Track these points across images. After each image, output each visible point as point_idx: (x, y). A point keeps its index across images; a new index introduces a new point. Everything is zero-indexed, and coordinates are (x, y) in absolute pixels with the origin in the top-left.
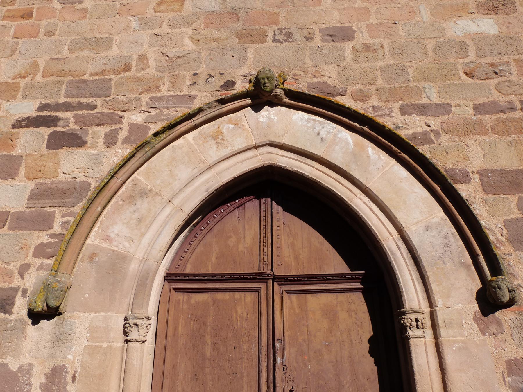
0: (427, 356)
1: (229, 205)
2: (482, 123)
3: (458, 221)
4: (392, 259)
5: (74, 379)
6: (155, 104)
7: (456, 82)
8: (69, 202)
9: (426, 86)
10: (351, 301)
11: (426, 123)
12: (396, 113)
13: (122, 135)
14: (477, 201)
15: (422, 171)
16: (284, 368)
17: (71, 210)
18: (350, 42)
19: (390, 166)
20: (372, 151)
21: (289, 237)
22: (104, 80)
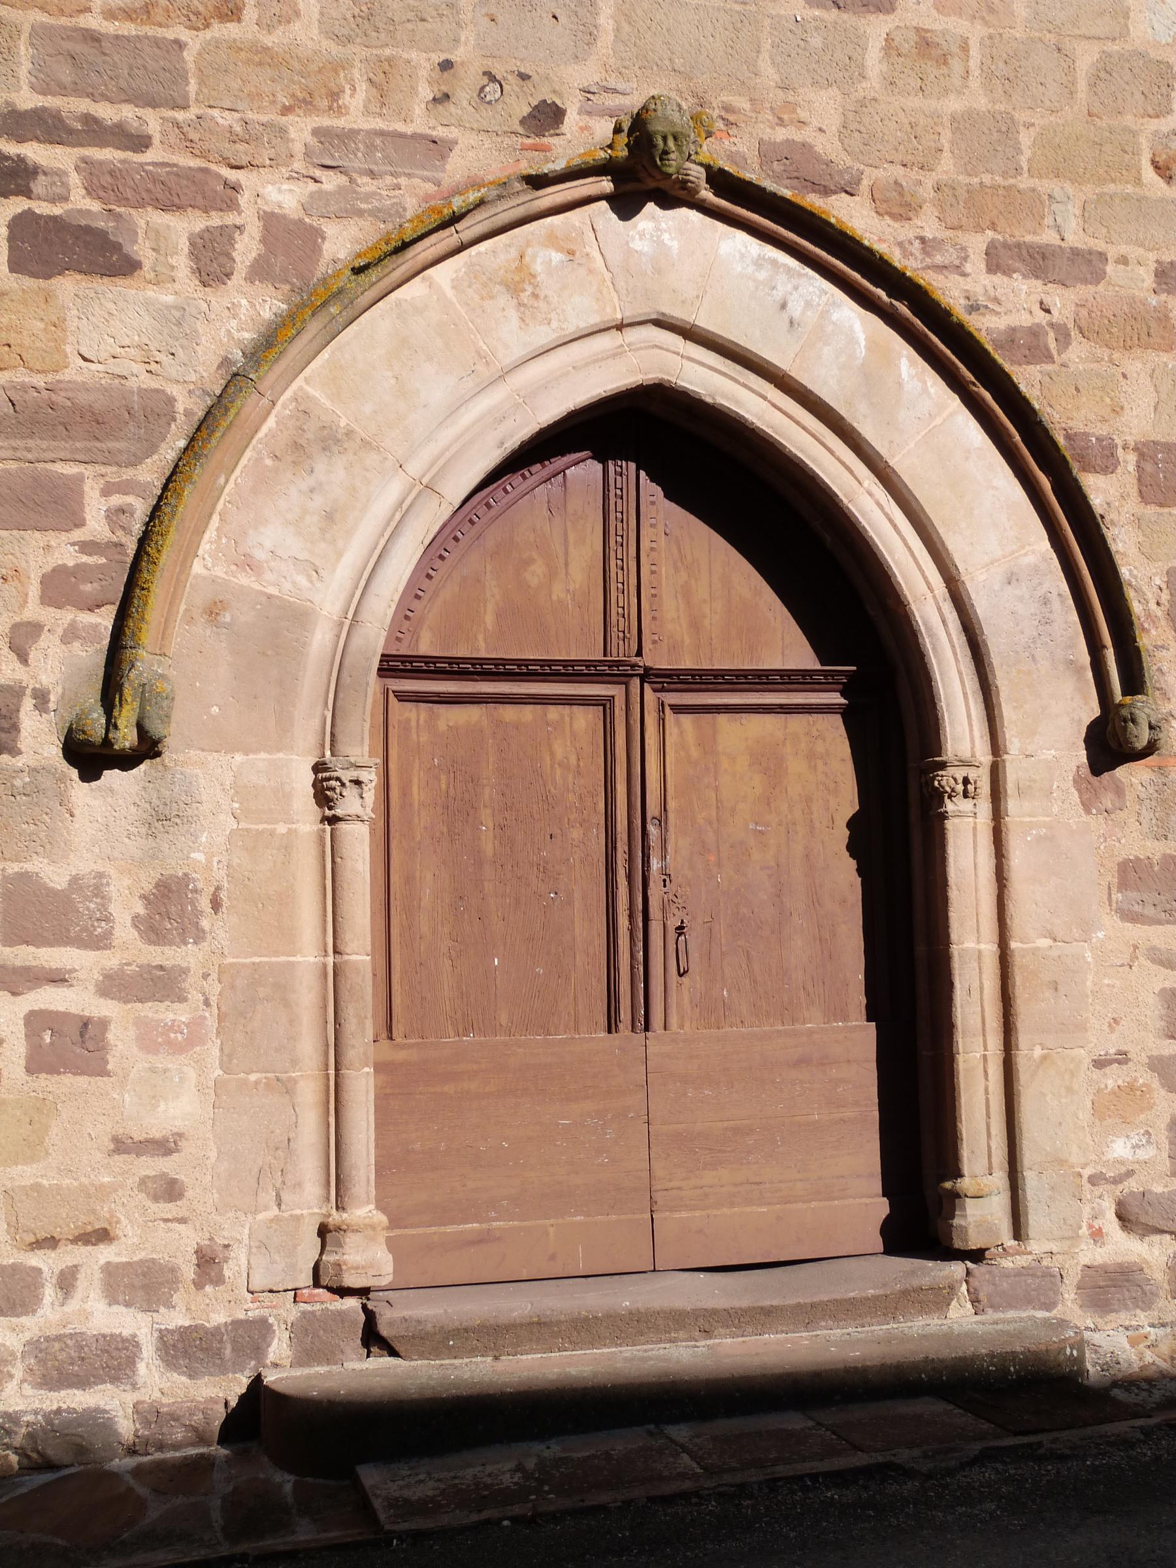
0: (975, 852)
1: (527, 473)
2: (1167, 317)
3: (1077, 565)
4: (929, 646)
5: (216, 904)
6: (333, 156)
7: (1129, 189)
8: (120, 451)
9: (1057, 193)
10: (815, 734)
11: (1041, 303)
12: (976, 264)
13: (247, 249)
14: (1123, 520)
15: (1017, 438)
16: (664, 881)
17: (128, 474)
18: (881, 16)
19: (947, 413)
20: (909, 366)
21: (677, 570)
22: (157, 43)
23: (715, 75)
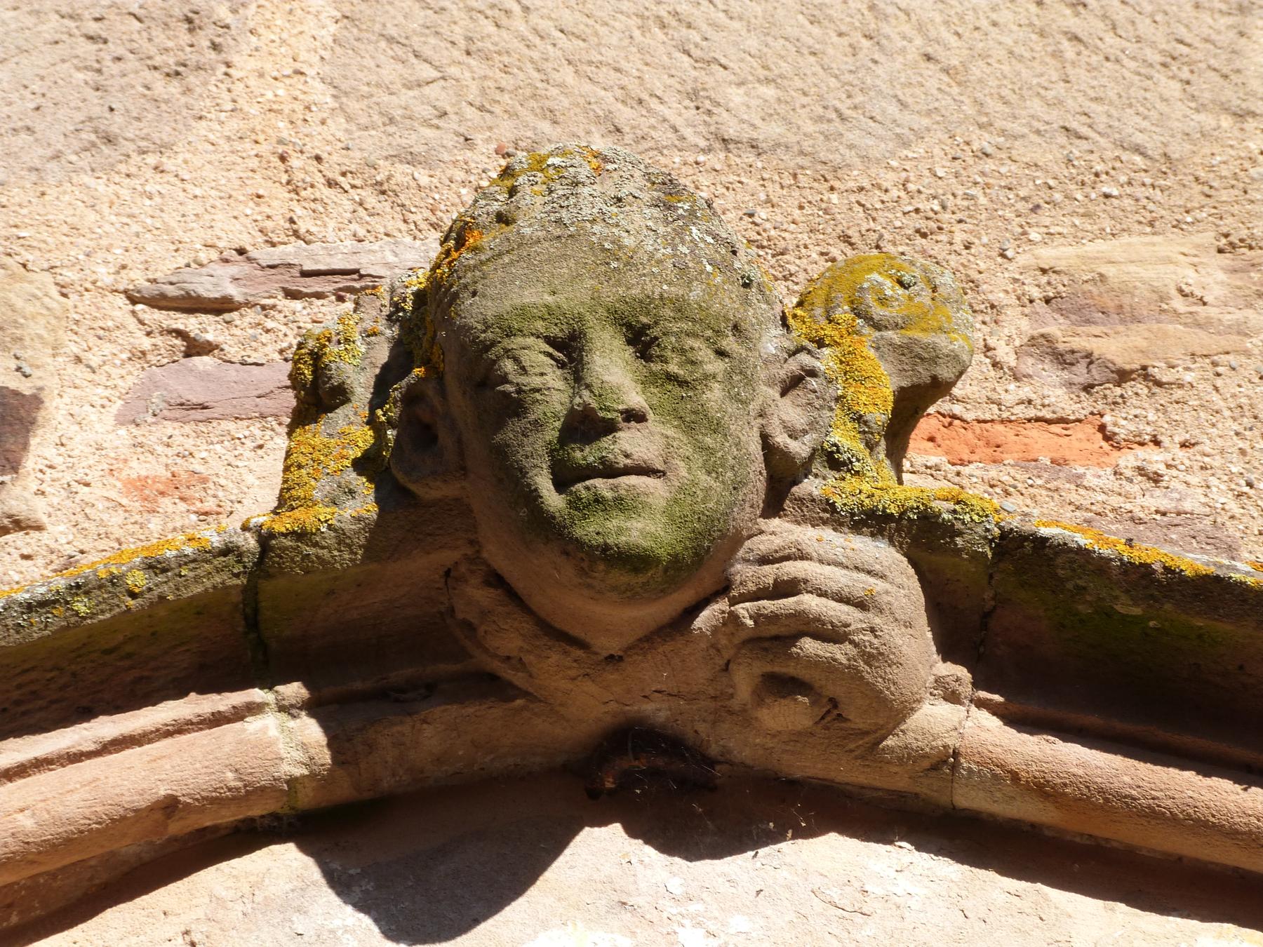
23: (983, 140)
